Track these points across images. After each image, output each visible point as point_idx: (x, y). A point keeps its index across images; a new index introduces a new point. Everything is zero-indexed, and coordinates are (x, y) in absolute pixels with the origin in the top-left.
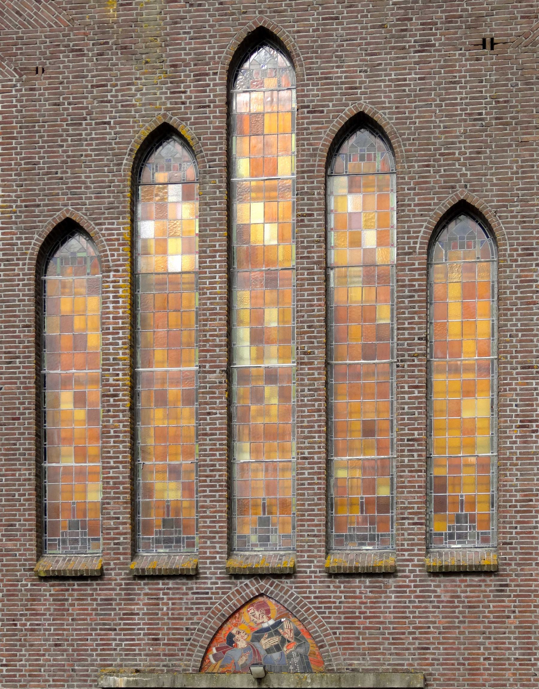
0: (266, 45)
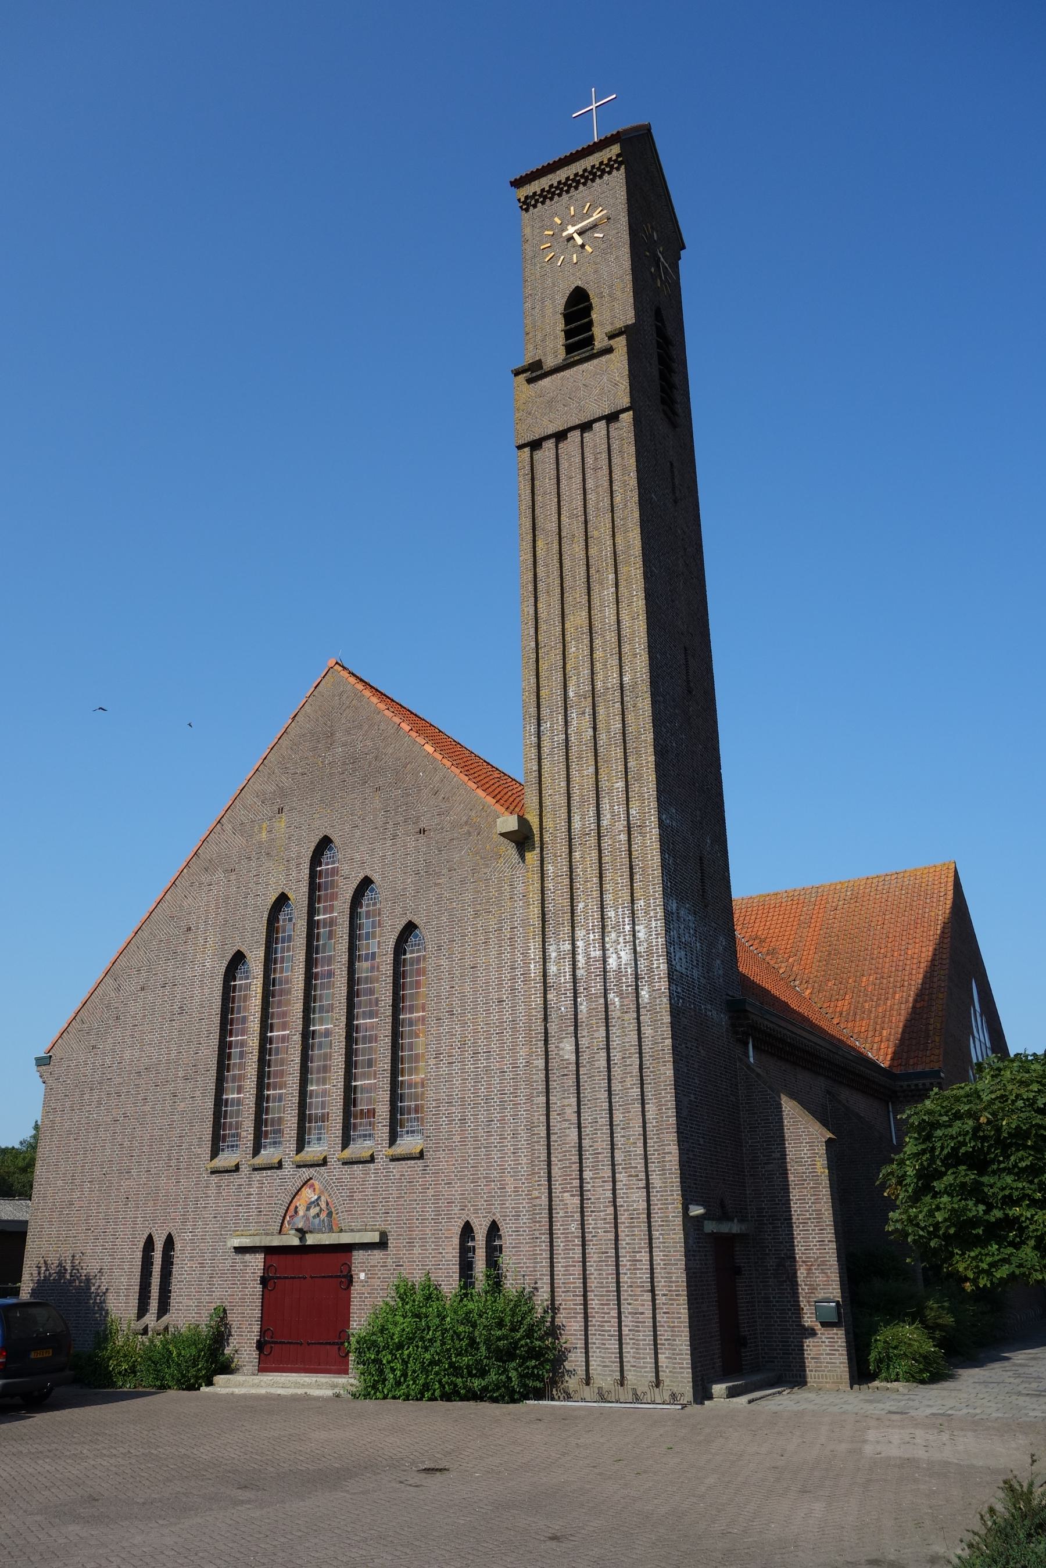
0: (739, 972)
